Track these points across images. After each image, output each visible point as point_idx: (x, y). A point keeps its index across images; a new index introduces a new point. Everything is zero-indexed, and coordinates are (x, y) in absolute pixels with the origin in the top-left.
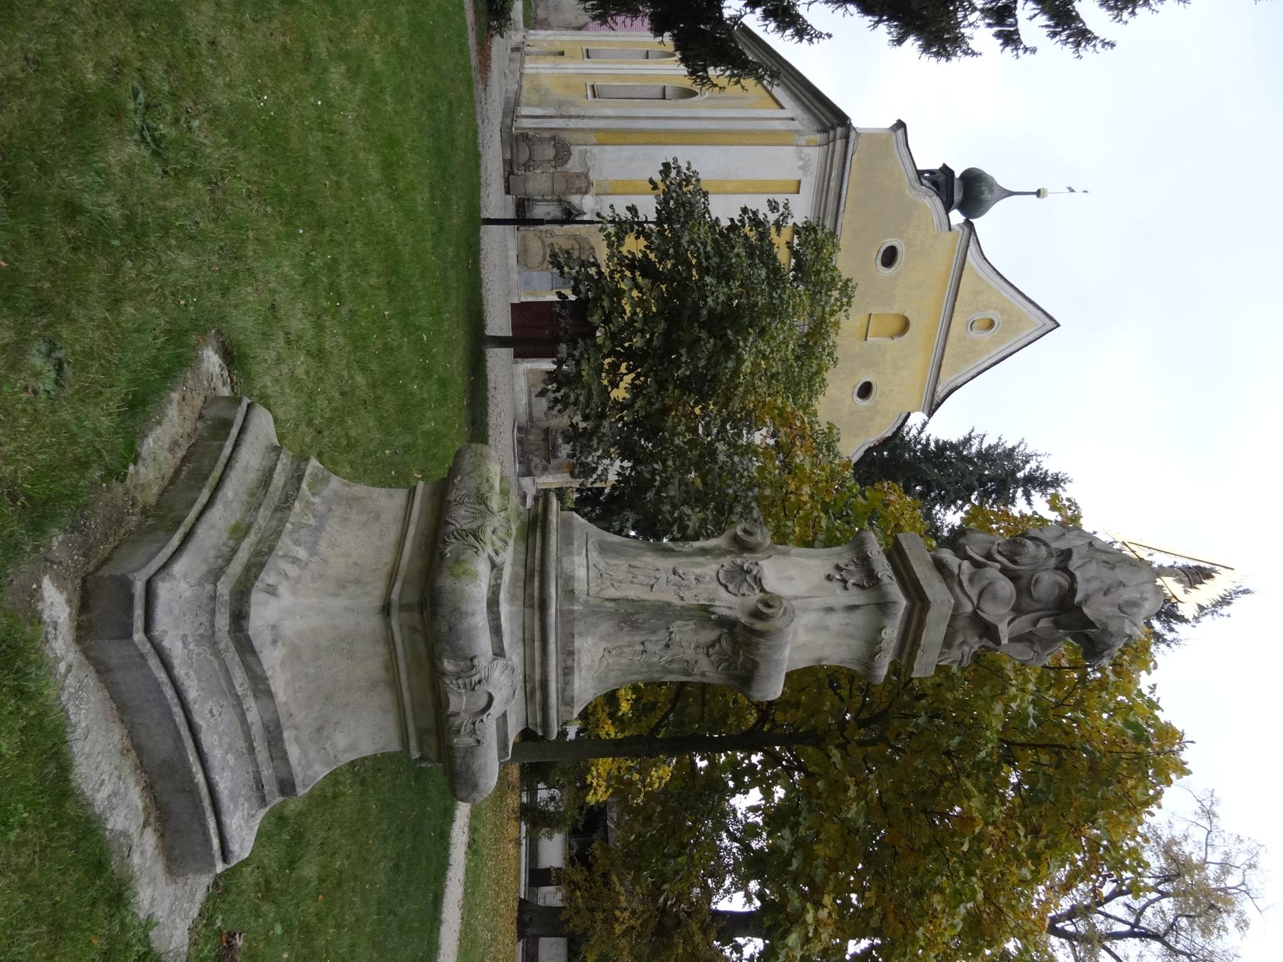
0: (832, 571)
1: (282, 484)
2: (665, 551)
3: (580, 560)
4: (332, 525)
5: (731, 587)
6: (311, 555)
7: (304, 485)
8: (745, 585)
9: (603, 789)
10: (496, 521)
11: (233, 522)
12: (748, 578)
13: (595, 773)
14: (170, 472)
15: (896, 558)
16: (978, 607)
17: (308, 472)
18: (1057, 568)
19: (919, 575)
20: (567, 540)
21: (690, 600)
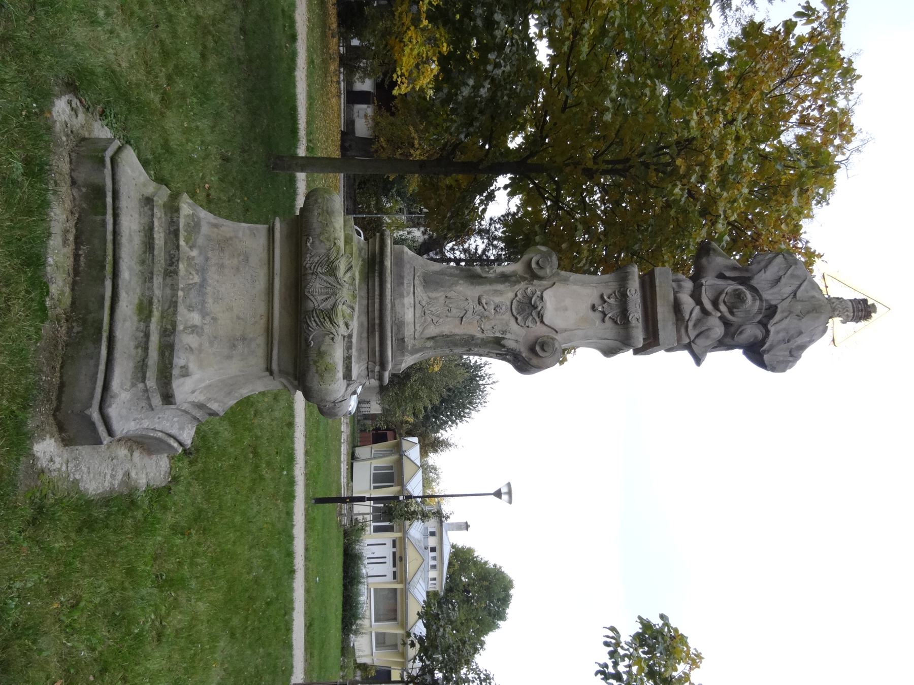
0: (597, 301)
1: (162, 242)
3: (408, 300)
4: (212, 276)
5: (520, 318)
6: (203, 318)
7: (182, 243)
8: (530, 318)
9: (405, 85)
10: (345, 294)
11: (136, 301)
12: (534, 314)
14: (70, 262)
15: (648, 288)
16: (693, 342)
17: (181, 226)
18: (760, 322)
19: (660, 317)
20: (399, 280)
21: (489, 334)
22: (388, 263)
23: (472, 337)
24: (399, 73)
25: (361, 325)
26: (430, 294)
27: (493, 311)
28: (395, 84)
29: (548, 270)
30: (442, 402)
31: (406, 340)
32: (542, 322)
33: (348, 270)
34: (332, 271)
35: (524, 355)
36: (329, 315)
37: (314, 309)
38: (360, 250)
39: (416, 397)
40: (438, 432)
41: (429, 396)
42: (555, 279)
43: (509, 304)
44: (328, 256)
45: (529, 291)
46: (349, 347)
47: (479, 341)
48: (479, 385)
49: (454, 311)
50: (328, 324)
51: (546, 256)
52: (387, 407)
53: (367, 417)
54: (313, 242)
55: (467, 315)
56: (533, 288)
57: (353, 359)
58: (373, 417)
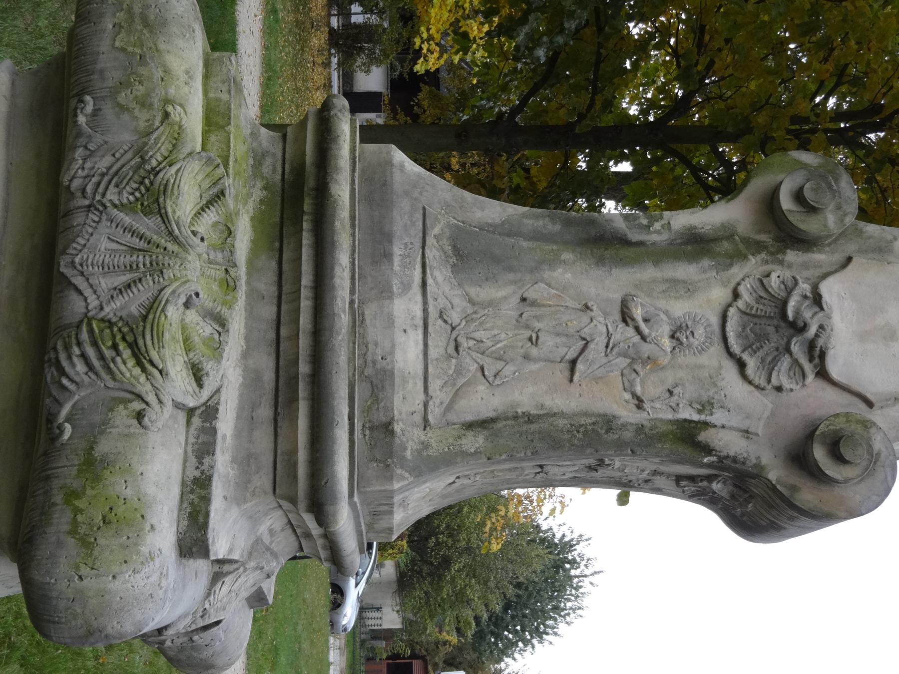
2: (605, 245)
3: (406, 307)
5: (752, 363)
8: (786, 361)
9: (436, 55)
10: (194, 271)
12: (795, 348)
13: (425, 36)
20: (377, 245)
21: (660, 412)
22: (342, 190)
23: (609, 422)
24: (425, 36)
25: (252, 380)
26: (473, 291)
27: (667, 343)
28: (418, 53)
29: (831, 219)
30: (506, 608)
31: (397, 428)
32: (822, 374)
33: (210, 203)
34: (153, 197)
35: (772, 476)
36: (135, 337)
37: (87, 318)
38: (259, 158)
39: (461, 598)
40: (499, 660)
41: (483, 597)
42: (850, 247)
43: (715, 321)
44: (141, 152)
45: (774, 282)
46: (204, 448)
47: (628, 435)
48: (571, 578)
49: (548, 341)
50: (127, 368)
51: (823, 177)
52: (410, 616)
53: (377, 635)
54: (96, 112)
55: (590, 353)
56: (787, 274)
57: (218, 490)
58: (388, 635)
